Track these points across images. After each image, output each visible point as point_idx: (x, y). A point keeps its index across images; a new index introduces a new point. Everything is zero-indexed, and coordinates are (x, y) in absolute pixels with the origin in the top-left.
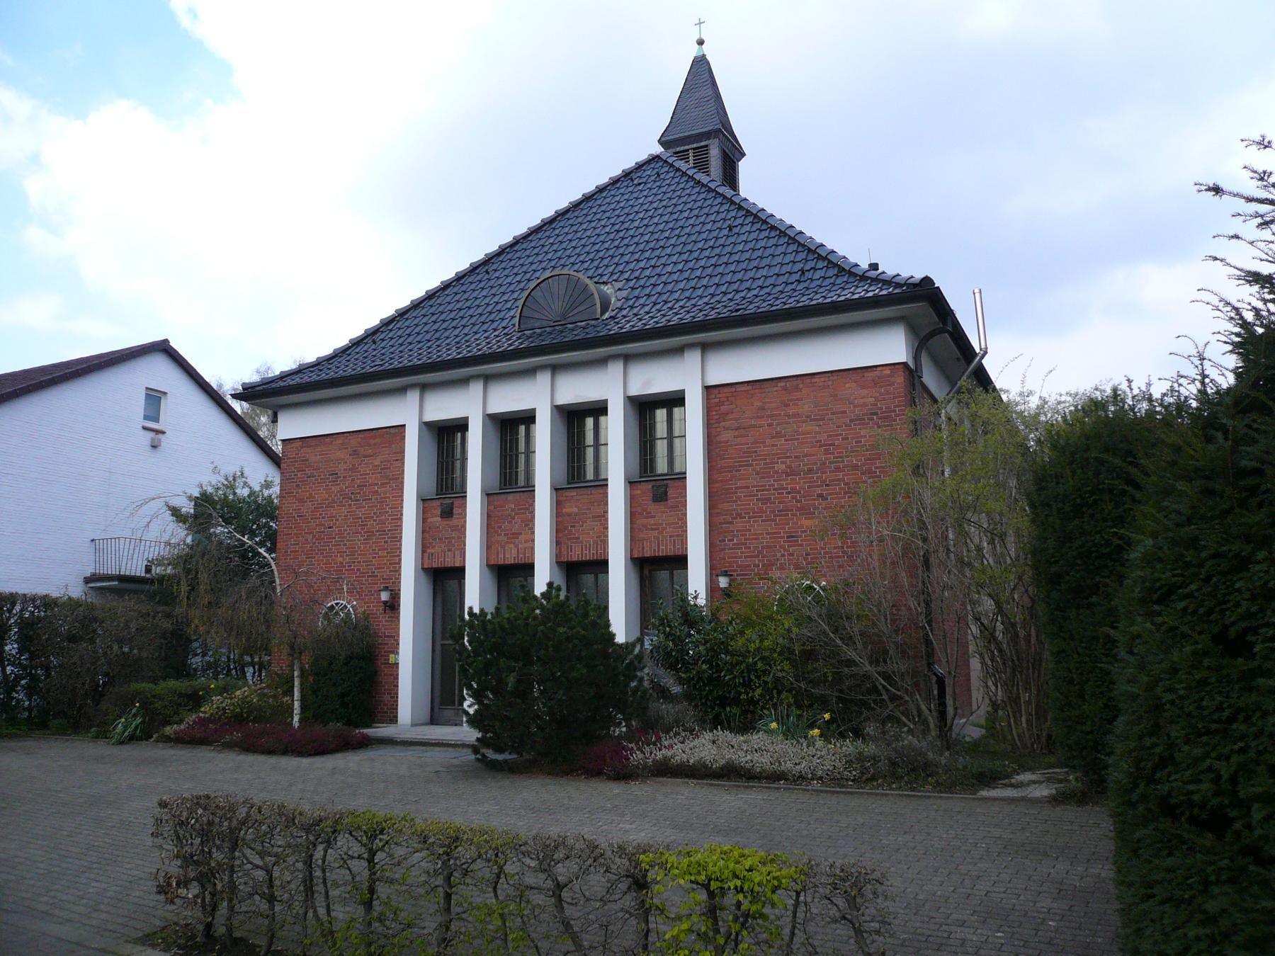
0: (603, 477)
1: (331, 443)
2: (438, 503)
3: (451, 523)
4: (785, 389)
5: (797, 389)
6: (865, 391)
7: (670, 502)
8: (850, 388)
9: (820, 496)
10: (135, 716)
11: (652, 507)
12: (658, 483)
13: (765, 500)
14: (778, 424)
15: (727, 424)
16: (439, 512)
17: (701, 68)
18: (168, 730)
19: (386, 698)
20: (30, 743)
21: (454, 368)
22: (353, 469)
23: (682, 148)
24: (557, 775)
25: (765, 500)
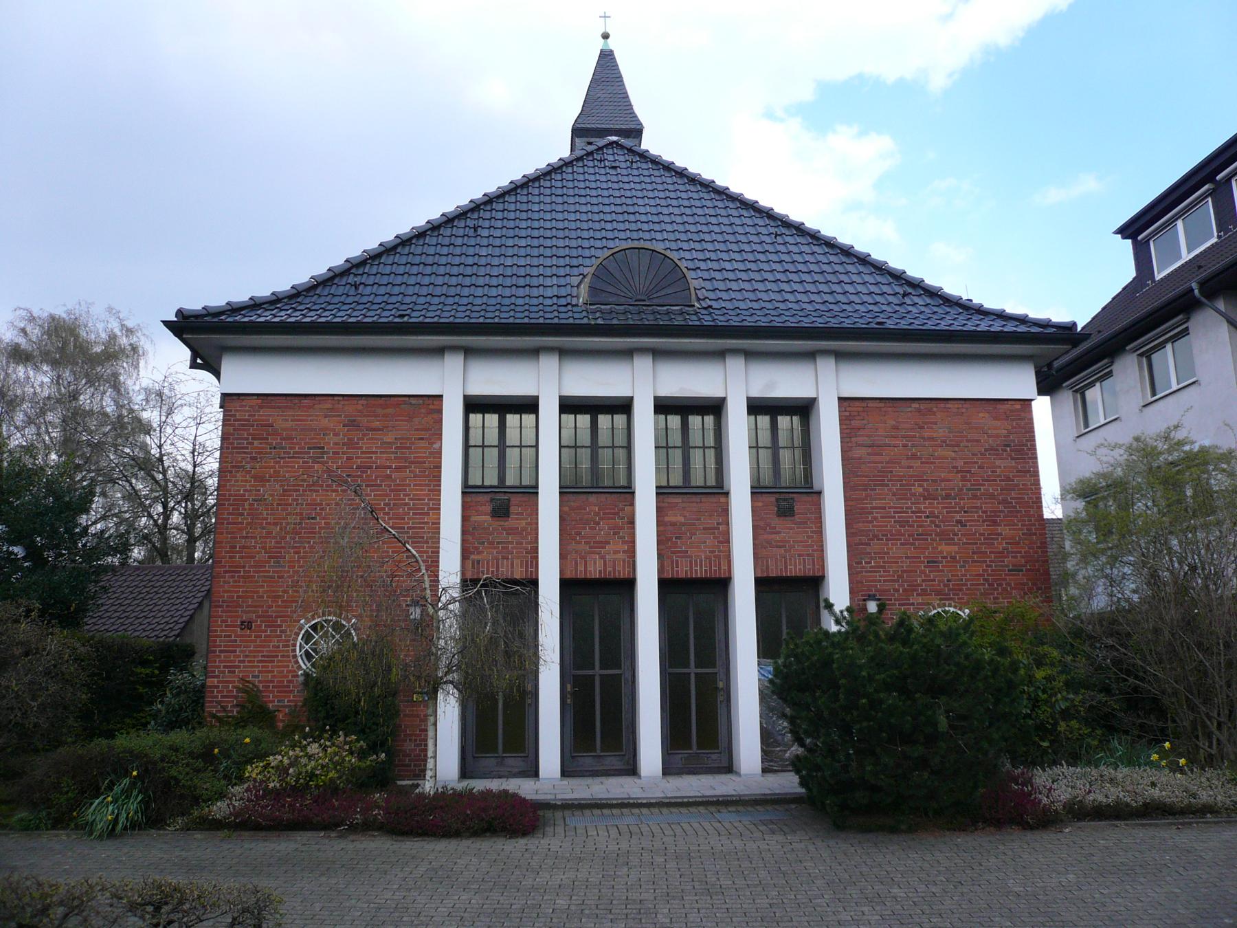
0: (816, 488)
1: (310, 407)
2: (487, 497)
3: (506, 524)
4: (919, 410)
5: (930, 410)
6: (998, 423)
7: (797, 518)
8: (983, 418)
9: (959, 522)
10: (127, 793)
11: (776, 522)
12: (782, 496)
13: (903, 523)
14: (913, 445)
15: (860, 440)
16: (488, 508)
17: (607, 60)
18: (220, 809)
19: (409, 746)
20: (961, 839)
21: (997, 342)
22: (350, 444)
24: (912, 829)
25: (903, 523)
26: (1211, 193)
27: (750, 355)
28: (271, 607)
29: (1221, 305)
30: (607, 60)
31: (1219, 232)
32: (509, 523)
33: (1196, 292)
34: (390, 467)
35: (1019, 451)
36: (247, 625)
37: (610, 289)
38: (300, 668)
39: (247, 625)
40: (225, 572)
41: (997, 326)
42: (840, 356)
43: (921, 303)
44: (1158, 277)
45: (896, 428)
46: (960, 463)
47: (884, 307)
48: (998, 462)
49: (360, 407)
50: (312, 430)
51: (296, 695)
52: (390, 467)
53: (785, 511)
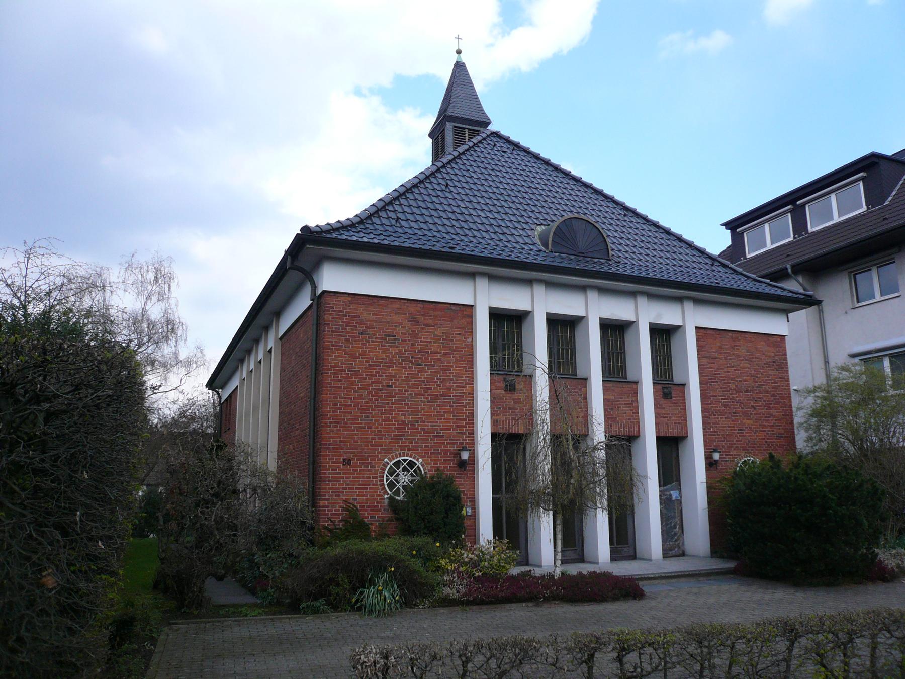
4: (732, 338)
8: (762, 345)
9: (753, 406)
13: (725, 406)
17: (459, 67)
21: (750, 297)
22: (413, 335)
23: (461, 126)
26: (791, 211)
27: (493, 278)
28: (363, 449)
29: (800, 279)
30: (459, 67)
31: (794, 235)
32: (515, 396)
33: (790, 270)
34: (440, 353)
35: (780, 366)
36: (347, 462)
37: (564, 244)
38: (386, 493)
39: (347, 462)
40: (330, 423)
41: (784, 293)
42: (492, 278)
43: (522, 241)
44: (749, 256)
45: (720, 347)
46: (752, 371)
47: (416, 231)
48: (770, 372)
49: (419, 309)
50: (388, 322)
51: (383, 513)
52: (440, 353)
53: (511, 388)
